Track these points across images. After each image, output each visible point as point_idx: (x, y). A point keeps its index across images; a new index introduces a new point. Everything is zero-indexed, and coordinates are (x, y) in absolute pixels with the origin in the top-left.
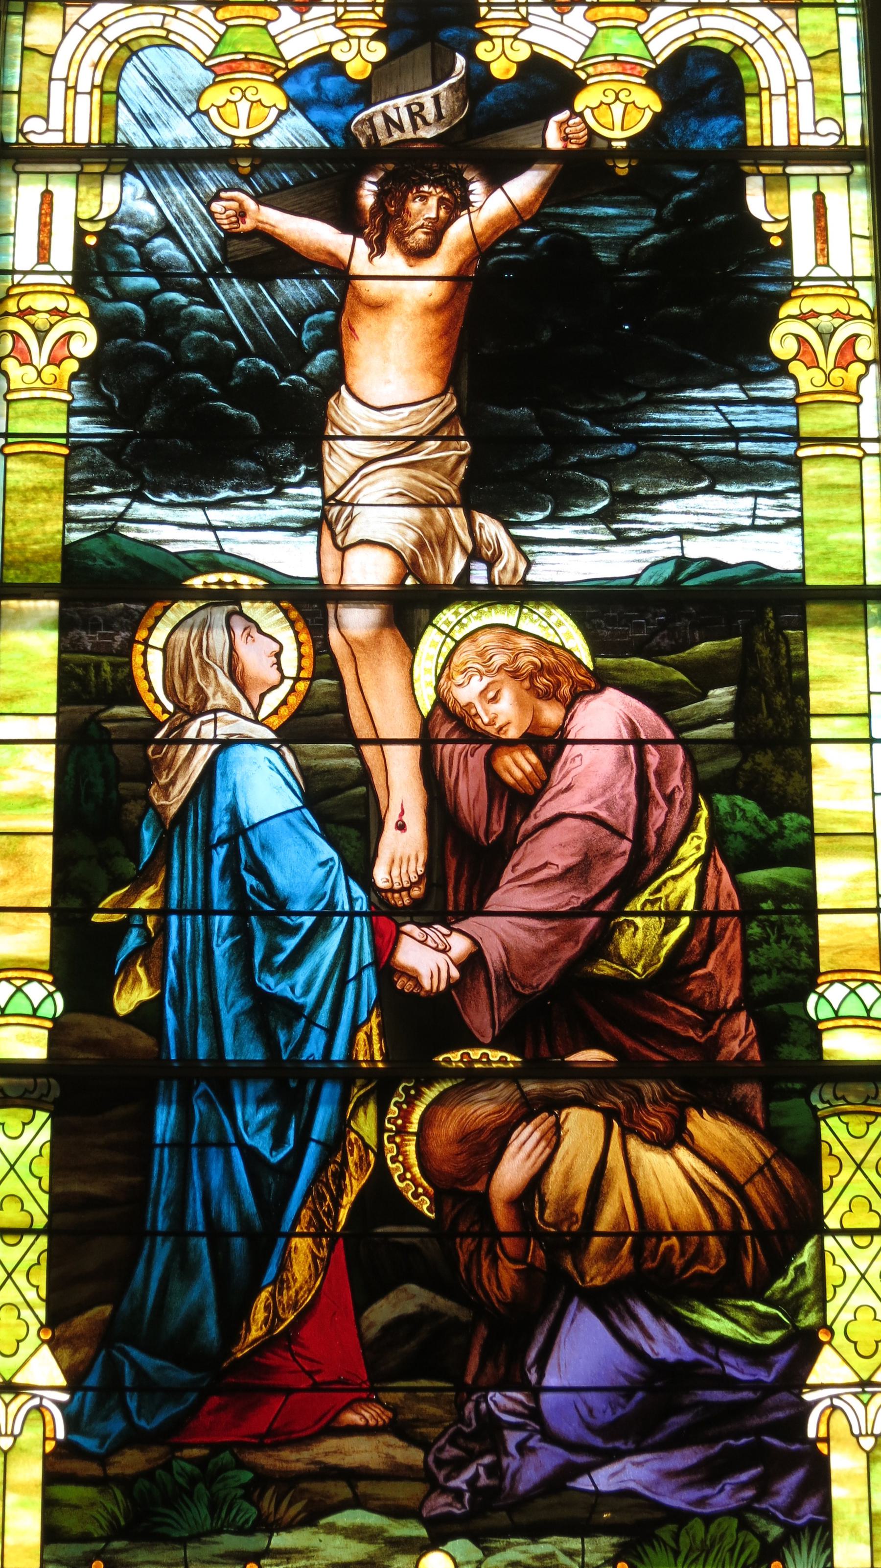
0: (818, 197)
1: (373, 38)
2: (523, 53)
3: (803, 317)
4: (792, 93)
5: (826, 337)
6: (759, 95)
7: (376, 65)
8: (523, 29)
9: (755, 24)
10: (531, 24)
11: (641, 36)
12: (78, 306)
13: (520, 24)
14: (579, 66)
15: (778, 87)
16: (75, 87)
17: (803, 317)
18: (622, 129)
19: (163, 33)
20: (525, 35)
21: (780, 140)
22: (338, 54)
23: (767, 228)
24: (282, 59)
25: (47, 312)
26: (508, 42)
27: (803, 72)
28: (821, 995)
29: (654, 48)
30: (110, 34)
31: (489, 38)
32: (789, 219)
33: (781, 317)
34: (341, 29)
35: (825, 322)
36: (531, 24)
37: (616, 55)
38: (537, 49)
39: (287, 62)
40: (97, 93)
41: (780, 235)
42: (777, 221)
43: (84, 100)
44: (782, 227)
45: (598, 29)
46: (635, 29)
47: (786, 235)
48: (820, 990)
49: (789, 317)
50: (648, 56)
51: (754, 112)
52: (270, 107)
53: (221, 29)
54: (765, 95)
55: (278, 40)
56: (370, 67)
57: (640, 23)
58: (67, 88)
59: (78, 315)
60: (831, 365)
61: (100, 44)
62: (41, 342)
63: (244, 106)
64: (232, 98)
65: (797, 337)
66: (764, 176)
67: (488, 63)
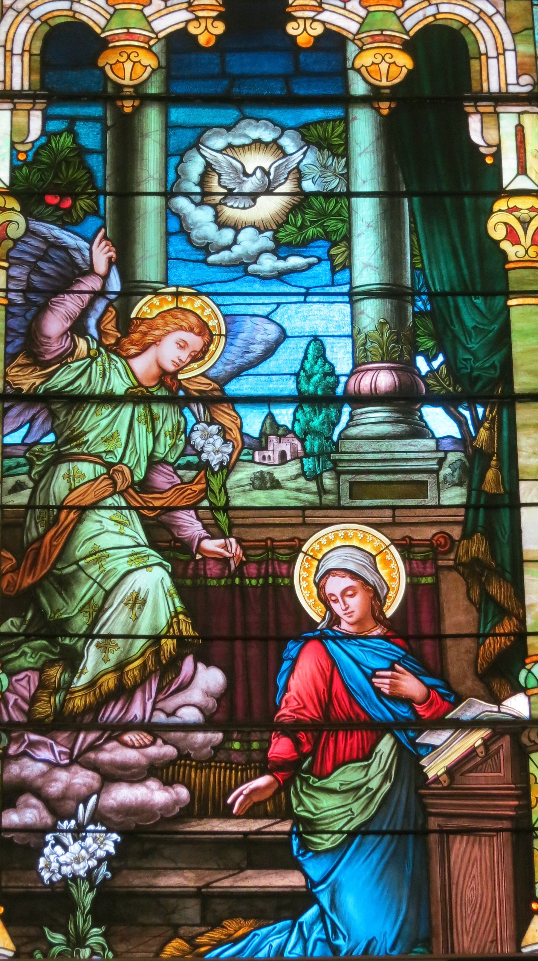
0: (519, 128)
1: (215, 19)
2: (318, 30)
3: (511, 210)
4: (501, 58)
5: (525, 224)
6: (480, 59)
7: (218, 37)
8: (319, 13)
9: (477, 10)
10: (324, 10)
11: (398, 17)
12: (12, 203)
13: (318, 9)
14: (357, 37)
15: (492, 53)
16: (11, 51)
17: (511, 210)
18: (387, 80)
19: (70, 13)
20: (320, 17)
21: (494, 88)
22: (192, 29)
23: (483, 150)
24: (153, 31)
25: (528, 209)
26: (308, 22)
27: (509, 45)
28: (529, 671)
29: (408, 24)
30: (36, 14)
31: (295, 19)
32: (499, 146)
33: (494, 211)
34: (192, 12)
35: (524, 214)
36: (324, 10)
37: (382, 30)
38: (328, 26)
39: (156, 34)
40: (26, 56)
41: (493, 155)
42: (489, 146)
43: (17, 60)
44: (494, 149)
45: (369, 12)
46: (394, 12)
47: (497, 156)
48: (528, 667)
49: (500, 210)
50: (403, 31)
51: (476, 71)
52: (402, 67)
53: (111, 10)
54: (483, 58)
55: (150, 19)
56: (312, 40)
57: (398, 8)
58: (6, 51)
59: (13, 209)
60: (529, 243)
61: (29, 21)
62: (525, 231)
63: (128, 66)
64: (376, 61)
65: (506, 224)
66: (482, 114)
67: (296, 36)
